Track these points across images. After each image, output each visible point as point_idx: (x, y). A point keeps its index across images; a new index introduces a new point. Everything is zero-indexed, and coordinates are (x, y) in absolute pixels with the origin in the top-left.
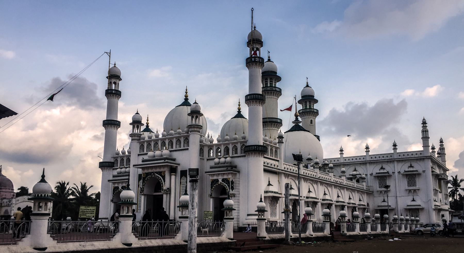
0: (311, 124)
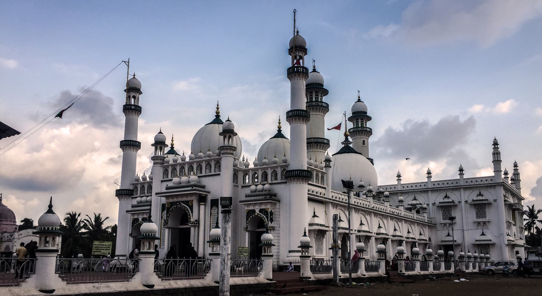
0: (363, 145)
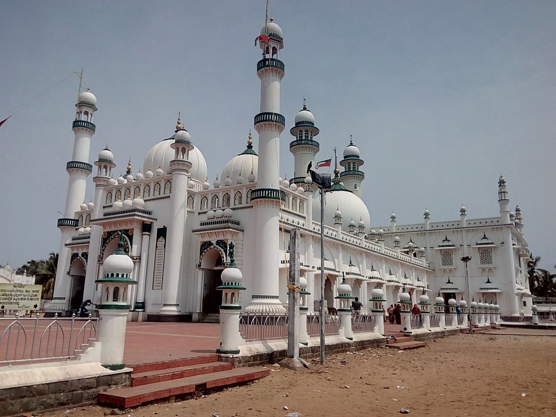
0: (355, 188)
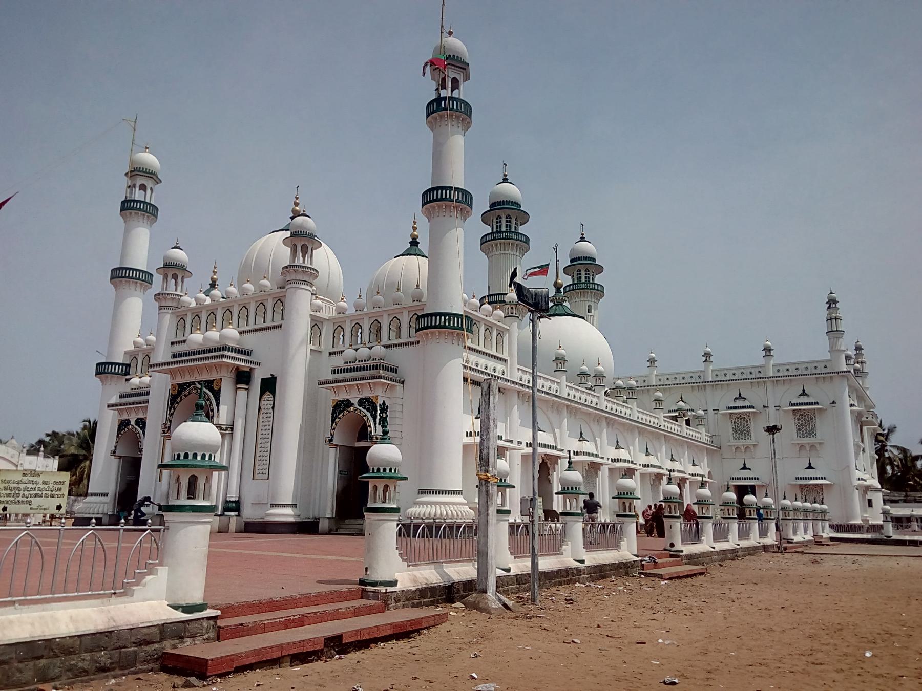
0: (589, 312)
